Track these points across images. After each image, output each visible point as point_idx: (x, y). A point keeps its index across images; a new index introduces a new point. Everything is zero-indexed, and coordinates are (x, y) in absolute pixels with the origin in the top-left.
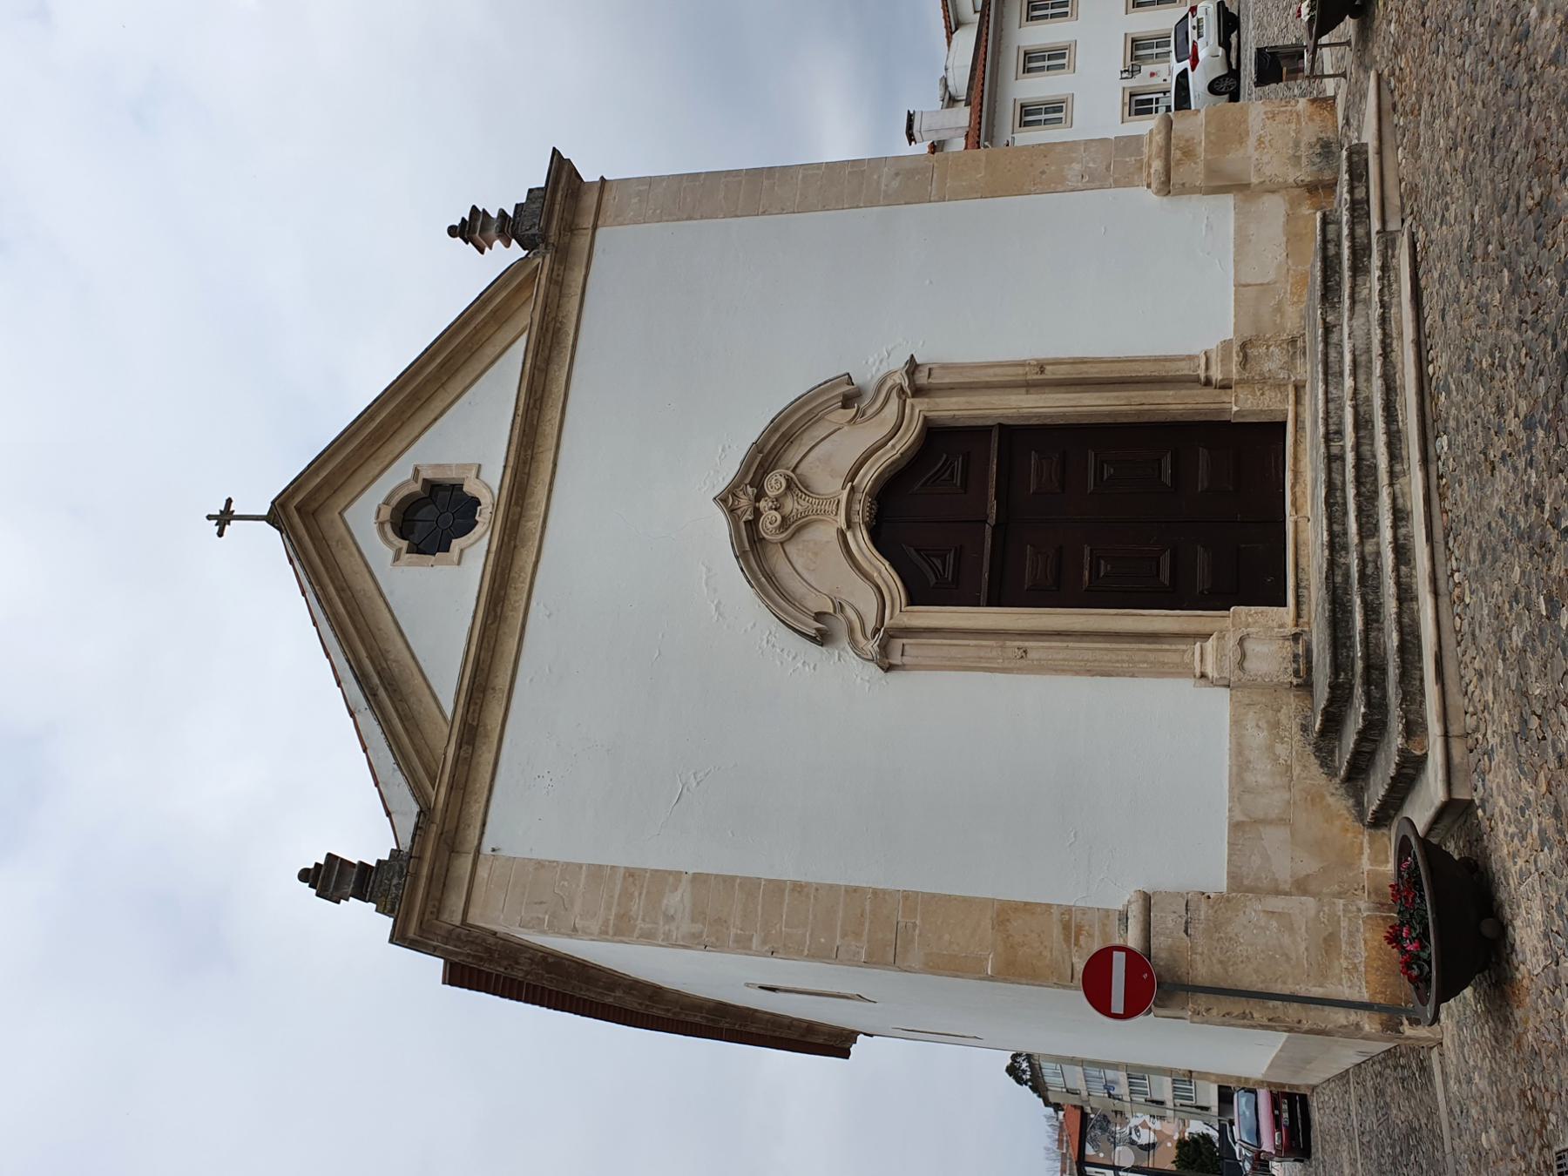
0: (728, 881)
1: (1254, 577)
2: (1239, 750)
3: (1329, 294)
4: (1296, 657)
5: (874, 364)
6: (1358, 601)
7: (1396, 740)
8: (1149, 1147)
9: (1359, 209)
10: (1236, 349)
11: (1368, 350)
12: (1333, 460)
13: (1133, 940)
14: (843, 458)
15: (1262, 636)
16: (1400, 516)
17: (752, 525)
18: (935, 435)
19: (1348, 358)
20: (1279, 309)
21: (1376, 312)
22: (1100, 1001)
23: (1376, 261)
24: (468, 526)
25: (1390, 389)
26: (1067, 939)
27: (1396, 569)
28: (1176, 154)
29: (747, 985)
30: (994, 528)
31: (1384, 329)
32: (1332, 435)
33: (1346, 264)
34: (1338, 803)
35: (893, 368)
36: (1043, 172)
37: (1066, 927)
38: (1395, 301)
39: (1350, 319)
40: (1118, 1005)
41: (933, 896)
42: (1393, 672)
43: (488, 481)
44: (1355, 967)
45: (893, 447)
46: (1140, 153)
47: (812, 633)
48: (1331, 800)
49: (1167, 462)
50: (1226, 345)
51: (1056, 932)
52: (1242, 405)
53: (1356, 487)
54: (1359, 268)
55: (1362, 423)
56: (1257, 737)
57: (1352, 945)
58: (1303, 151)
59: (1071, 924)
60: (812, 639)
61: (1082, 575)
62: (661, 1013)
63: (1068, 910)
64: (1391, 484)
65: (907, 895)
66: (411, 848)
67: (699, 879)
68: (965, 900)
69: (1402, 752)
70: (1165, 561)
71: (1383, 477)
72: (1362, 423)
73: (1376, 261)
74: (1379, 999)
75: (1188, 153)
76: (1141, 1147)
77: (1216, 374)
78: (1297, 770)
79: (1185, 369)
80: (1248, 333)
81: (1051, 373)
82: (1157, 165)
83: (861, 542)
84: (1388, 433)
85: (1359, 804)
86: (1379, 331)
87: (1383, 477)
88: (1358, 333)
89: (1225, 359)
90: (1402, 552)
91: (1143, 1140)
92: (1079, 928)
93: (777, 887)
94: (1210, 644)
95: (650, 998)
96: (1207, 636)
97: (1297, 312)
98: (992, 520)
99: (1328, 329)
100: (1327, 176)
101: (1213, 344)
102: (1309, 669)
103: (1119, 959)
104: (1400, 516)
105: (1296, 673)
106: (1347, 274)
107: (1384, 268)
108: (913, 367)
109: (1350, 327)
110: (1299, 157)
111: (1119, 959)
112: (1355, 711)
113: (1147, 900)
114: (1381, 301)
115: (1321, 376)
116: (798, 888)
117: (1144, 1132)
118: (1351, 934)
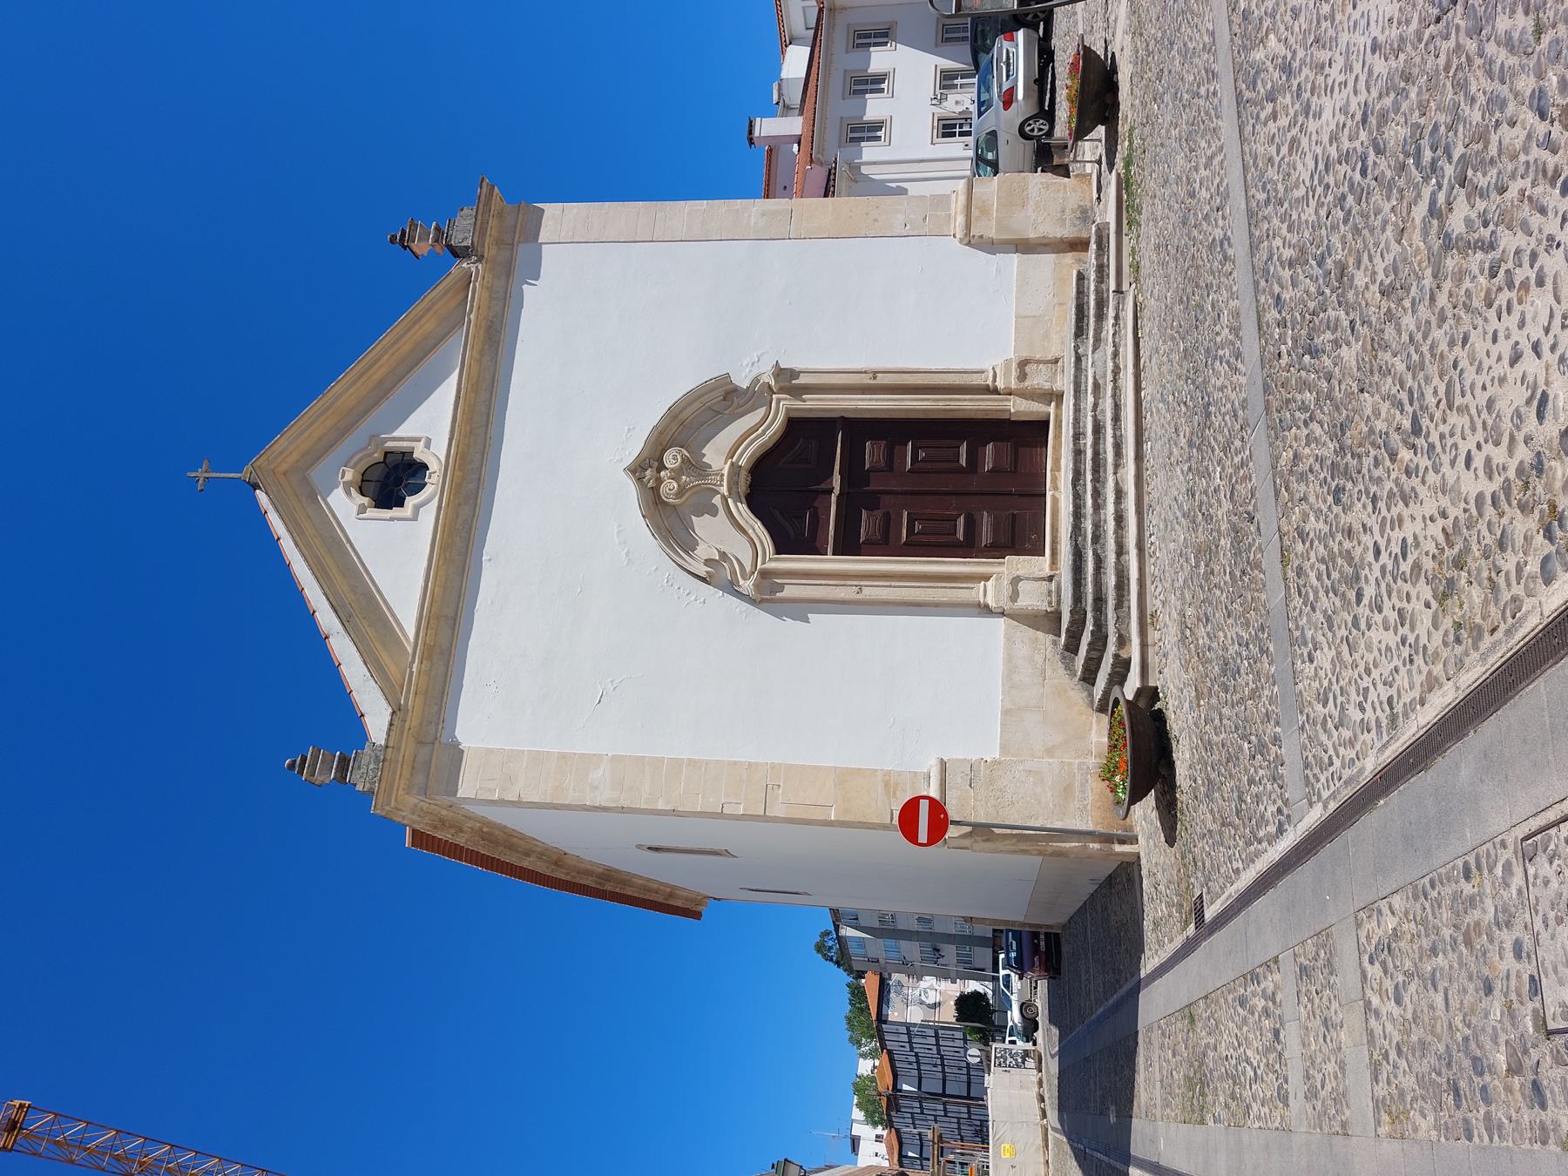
0: (640, 760)
1: (1020, 535)
2: (1009, 658)
3: (1080, 332)
4: (1050, 592)
6: (1090, 553)
7: (1111, 648)
8: (935, 1006)
9: (1101, 269)
10: (1014, 365)
11: (1105, 376)
12: (1078, 453)
13: (934, 793)
14: (729, 449)
15: (1029, 578)
16: (1119, 494)
17: (655, 490)
18: (796, 426)
19: (1090, 381)
20: (1046, 336)
21: (1110, 350)
22: (911, 835)
23: (1111, 313)
25: (1117, 407)
27: (1116, 532)
28: (975, 212)
29: (639, 846)
30: (838, 497)
32: (1077, 436)
33: (1092, 312)
34: (1077, 694)
37: (887, 785)
42: (1111, 603)
43: (435, 452)
45: (764, 432)
47: (703, 574)
48: (1072, 693)
49: (964, 449)
51: (880, 788)
52: (1019, 408)
53: (1091, 470)
54: (1100, 316)
55: (1098, 429)
56: (1022, 650)
57: (1083, 792)
58: (1068, 215)
60: (703, 580)
62: (563, 877)
65: (773, 766)
66: (387, 740)
69: (1116, 656)
71: (1110, 469)
72: (1098, 429)
73: (1111, 313)
74: (1100, 829)
75: (985, 211)
76: (929, 1006)
77: (1000, 384)
79: (977, 380)
80: (1025, 354)
81: (882, 380)
82: (961, 219)
83: (742, 511)
84: (1115, 436)
85: (1091, 695)
87: (1110, 469)
88: (1099, 364)
90: (1120, 519)
91: (931, 1001)
92: (896, 784)
93: (677, 763)
94: (990, 584)
95: (556, 864)
96: (987, 578)
97: (1060, 341)
98: (837, 491)
99: (1078, 359)
100: (1084, 235)
101: (998, 362)
103: (924, 806)
104: (1119, 494)
105: (1050, 603)
106: (1092, 320)
107: (1117, 318)
108: (779, 372)
111: (924, 806)
112: (1083, 632)
113: (943, 765)
117: (931, 994)
118: (1082, 785)
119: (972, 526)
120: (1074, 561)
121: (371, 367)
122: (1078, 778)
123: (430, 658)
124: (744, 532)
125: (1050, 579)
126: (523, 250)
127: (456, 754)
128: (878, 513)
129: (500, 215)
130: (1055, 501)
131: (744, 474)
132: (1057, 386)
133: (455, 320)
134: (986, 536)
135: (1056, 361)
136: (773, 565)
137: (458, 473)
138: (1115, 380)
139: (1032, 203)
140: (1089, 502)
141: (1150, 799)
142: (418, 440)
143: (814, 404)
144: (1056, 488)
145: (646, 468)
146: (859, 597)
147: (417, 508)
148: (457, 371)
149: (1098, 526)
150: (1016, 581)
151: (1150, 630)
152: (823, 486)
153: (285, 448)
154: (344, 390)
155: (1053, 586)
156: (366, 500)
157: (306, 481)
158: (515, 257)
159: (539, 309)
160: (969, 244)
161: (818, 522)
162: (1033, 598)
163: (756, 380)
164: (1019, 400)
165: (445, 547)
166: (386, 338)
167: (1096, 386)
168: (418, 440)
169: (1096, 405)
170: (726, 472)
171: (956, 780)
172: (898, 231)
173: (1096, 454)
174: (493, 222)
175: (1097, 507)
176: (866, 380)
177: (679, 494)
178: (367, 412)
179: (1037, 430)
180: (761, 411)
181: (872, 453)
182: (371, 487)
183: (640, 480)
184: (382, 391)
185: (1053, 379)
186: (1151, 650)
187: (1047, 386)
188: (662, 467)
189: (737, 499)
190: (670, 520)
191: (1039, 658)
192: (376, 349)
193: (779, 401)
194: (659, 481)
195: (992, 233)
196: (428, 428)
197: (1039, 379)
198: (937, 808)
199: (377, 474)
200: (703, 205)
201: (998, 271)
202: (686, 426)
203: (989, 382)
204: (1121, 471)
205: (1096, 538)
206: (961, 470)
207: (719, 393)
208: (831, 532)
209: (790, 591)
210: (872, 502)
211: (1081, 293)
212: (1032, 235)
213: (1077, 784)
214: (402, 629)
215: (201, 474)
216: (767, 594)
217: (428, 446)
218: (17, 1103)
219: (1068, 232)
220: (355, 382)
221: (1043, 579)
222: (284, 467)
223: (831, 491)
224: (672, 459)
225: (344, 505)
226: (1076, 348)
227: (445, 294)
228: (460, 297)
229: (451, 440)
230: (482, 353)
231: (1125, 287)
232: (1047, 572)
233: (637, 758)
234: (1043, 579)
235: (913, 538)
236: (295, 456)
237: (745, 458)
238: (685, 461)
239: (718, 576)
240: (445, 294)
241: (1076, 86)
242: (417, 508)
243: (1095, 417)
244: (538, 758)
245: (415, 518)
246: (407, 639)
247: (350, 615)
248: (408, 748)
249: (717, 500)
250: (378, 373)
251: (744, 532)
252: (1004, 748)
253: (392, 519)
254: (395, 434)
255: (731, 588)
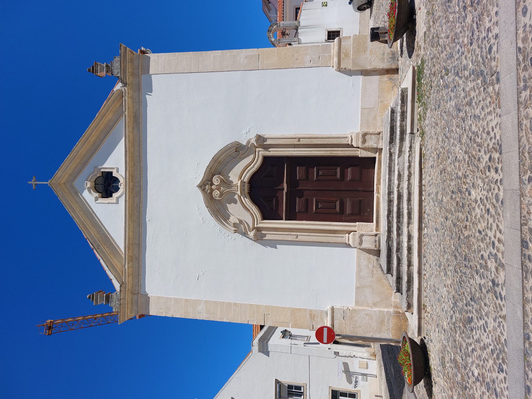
1: (363, 212)
2: (359, 265)
5: (245, 137)
13: (329, 325)
14: (240, 173)
16: (410, 237)
24: (117, 189)
26: (311, 318)
27: (408, 256)
28: (343, 56)
31: (409, 171)
35: (251, 137)
36: (297, 59)
37: (311, 315)
38: (413, 160)
39: (398, 158)
40: (325, 340)
41: (274, 307)
43: (120, 174)
44: (389, 329)
46: (330, 52)
48: (384, 281)
49: (338, 170)
50: (358, 134)
51: (308, 316)
55: (400, 197)
56: (364, 262)
57: (388, 323)
58: (386, 56)
59: (312, 315)
61: (313, 208)
63: (311, 310)
64: (408, 227)
65: (266, 307)
67: (206, 302)
68: (282, 308)
70: (338, 203)
75: (347, 55)
78: (375, 272)
79: (344, 142)
80: (365, 130)
81: (303, 142)
82: (336, 59)
83: (247, 202)
84: (408, 209)
86: (407, 172)
88: (401, 164)
89: (357, 140)
92: (314, 315)
93: (229, 304)
96: (349, 232)
98: (285, 190)
102: (379, 246)
103: (325, 330)
104: (410, 237)
105: (376, 246)
107: (411, 147)
109: (398, 161)
110: (384, 59)
111: (325, 330)
113: (333, 309)
114: (409, 160)
115: (387, 172)
116: (235, 304)
118: (388, 320)
119: (342, 205)
120: (388, 253)
121: (89, 137)
122: (386, 317)
123: (132, 261)
124: (249, 210)
125: (376, 235)
126: (143, 77)
127: (147, 299)
128: (303, 199)
129: (132, 60)
130: (378, 198)
131: (246, 185)
132: (380, 146)
133: (120, 114)
134: (348, 210)
135: (379, 134)
136: (260, 225)
137: (131, 184)
138: (409, 180)
139: (369, 50)
140: (395, 232)
141: (422, 383)
142: (114, 169)
143: (273, 152)
144: (378, 192)
145: (205, 185)
146: (297, 240)
147: (118, 199)
148: (123, 139)
149: (399, 244)
150: (361, 236)
151: (423, 312)
152: (279, 187)
153: (62, 174)
154: (80, 148)
155: (377, 238)
156: (97, 195)
157: (73, 187)
158: (141, 85)
159: (154, 103)
160: (340, 71)
161: (279, 203)
162: (368, 243)
163: (249, 142)
164: (362, 151)
165: (131, 216)
166: (92, 125)
167: (399, 175)
168: (114, 169)
169: (399, 185)
170: (239, 185)
171: (337, 316)
172: (307, 65)
173: (399, 209)
174: (129, 65)
175: (399, 235)
176: (296, 142)
177: (221, 196)
178: (91, 156)
179: (369, 163)
180: (252, 156)
181: (300, 172)
182: (100, 188)
183: (204, 190)
184: (96, 147)
185: (377, 142)
186: (423, 321)
187: (375, 146)
188: (212, 184)
189: (245, 197)
190: (218, 208)
191: (371, 266)
192: (89, 130)
193: (259, 151)
194: (212, 190)
195: (350, 67)
196: (116, 162)
197: (371, 143)
198: (330, 331)
199: (101, 181)
200: (218, 53)
201: (353, 85)
202: (219, 167)
203: (349, 143)
204: (411, 226)
205: (398, 250)
206: (337, 213)
207: (233, 150)
208: (284, 208)
209: (268, 237)
210: (300, 194)
211: (393, 120)
212: (369, 67)
213: (386, 320)
214: (118, 247)
215: (33, 182)
216: (259, 236)
217: (118, 171)
218: (49, 321)
219: (385, 65)
220: (84, 144)
221: (373, 235)
222: (63, 181)
223: (283, 189)
224: (216, 180)
225: (89, 197)
226: (390, 149)
227: (114, 102)
228: (120, 102)
229: (126, 171)
230: (133, 129)
231: (415, 131)
232: (374, 232)
233: (214, 302)
234: (373, 235)
235: (319, 178)
236: (66, 177)
237: (246, 178)
238: (222, 181)
239: (239, 228)
240: (114, 102)
241: (394, 22)
242: (118, 199)
243: (398, 191)
244: (177, 301)
245: (117, 203)
246: (122, 253)
247: (99, 246)
248: (129, 297)
249: (236, 197)
250: (93, 139)
251: (249, 210)
252: (357, 303)
253: (108, 203)
254: (104, 166)
255: (245, 234)
